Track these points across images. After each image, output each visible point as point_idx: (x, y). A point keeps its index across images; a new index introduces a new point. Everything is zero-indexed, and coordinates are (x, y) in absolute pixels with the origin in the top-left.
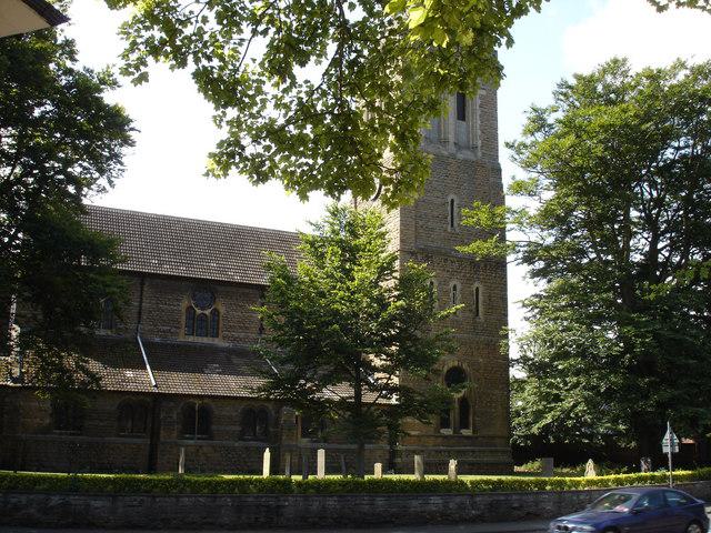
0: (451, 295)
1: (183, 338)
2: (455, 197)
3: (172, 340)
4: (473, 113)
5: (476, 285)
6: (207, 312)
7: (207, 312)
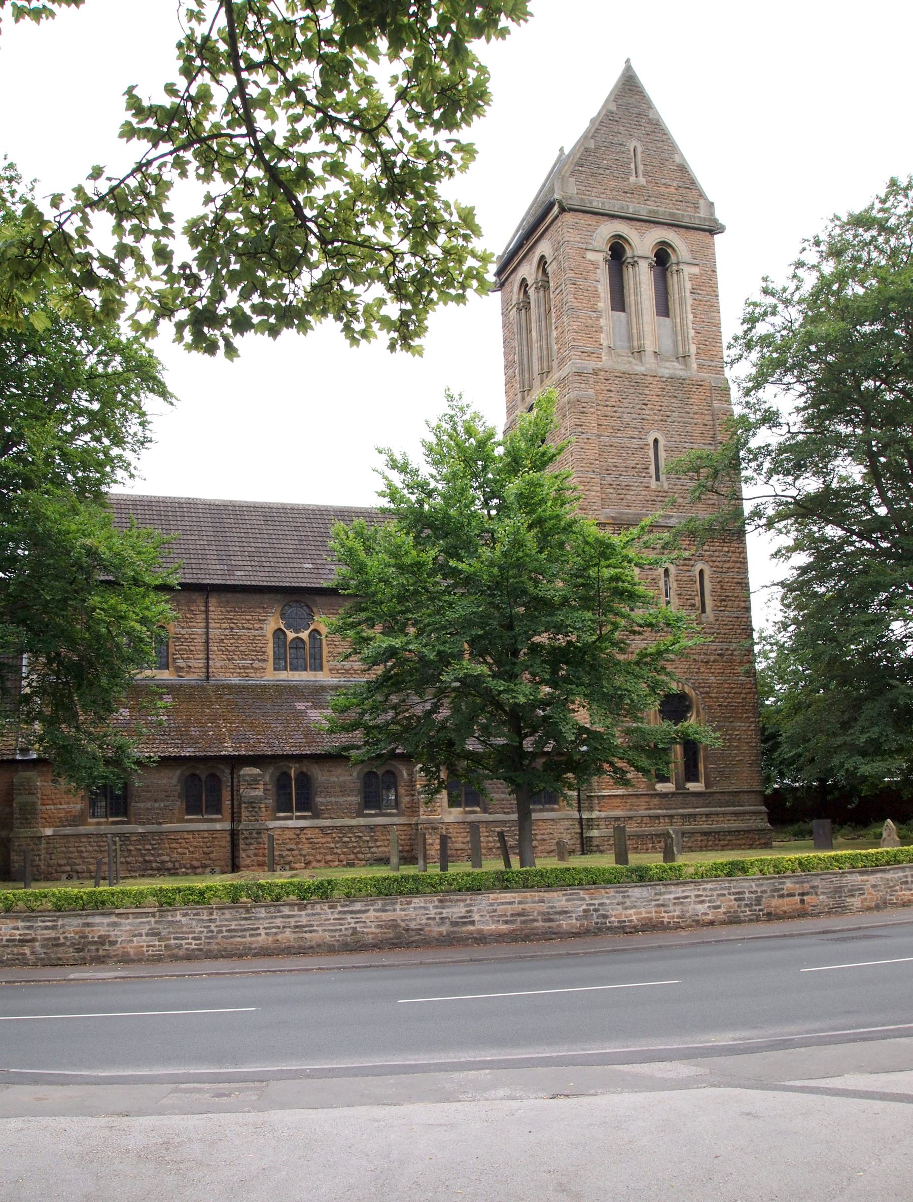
0: (662, 584)
1: (271, 676)
2: (656, 435)
3: (255, 679)
4: (681, 304)
5: (699, 566)
6: (304, 635)
7: (304, 635)
